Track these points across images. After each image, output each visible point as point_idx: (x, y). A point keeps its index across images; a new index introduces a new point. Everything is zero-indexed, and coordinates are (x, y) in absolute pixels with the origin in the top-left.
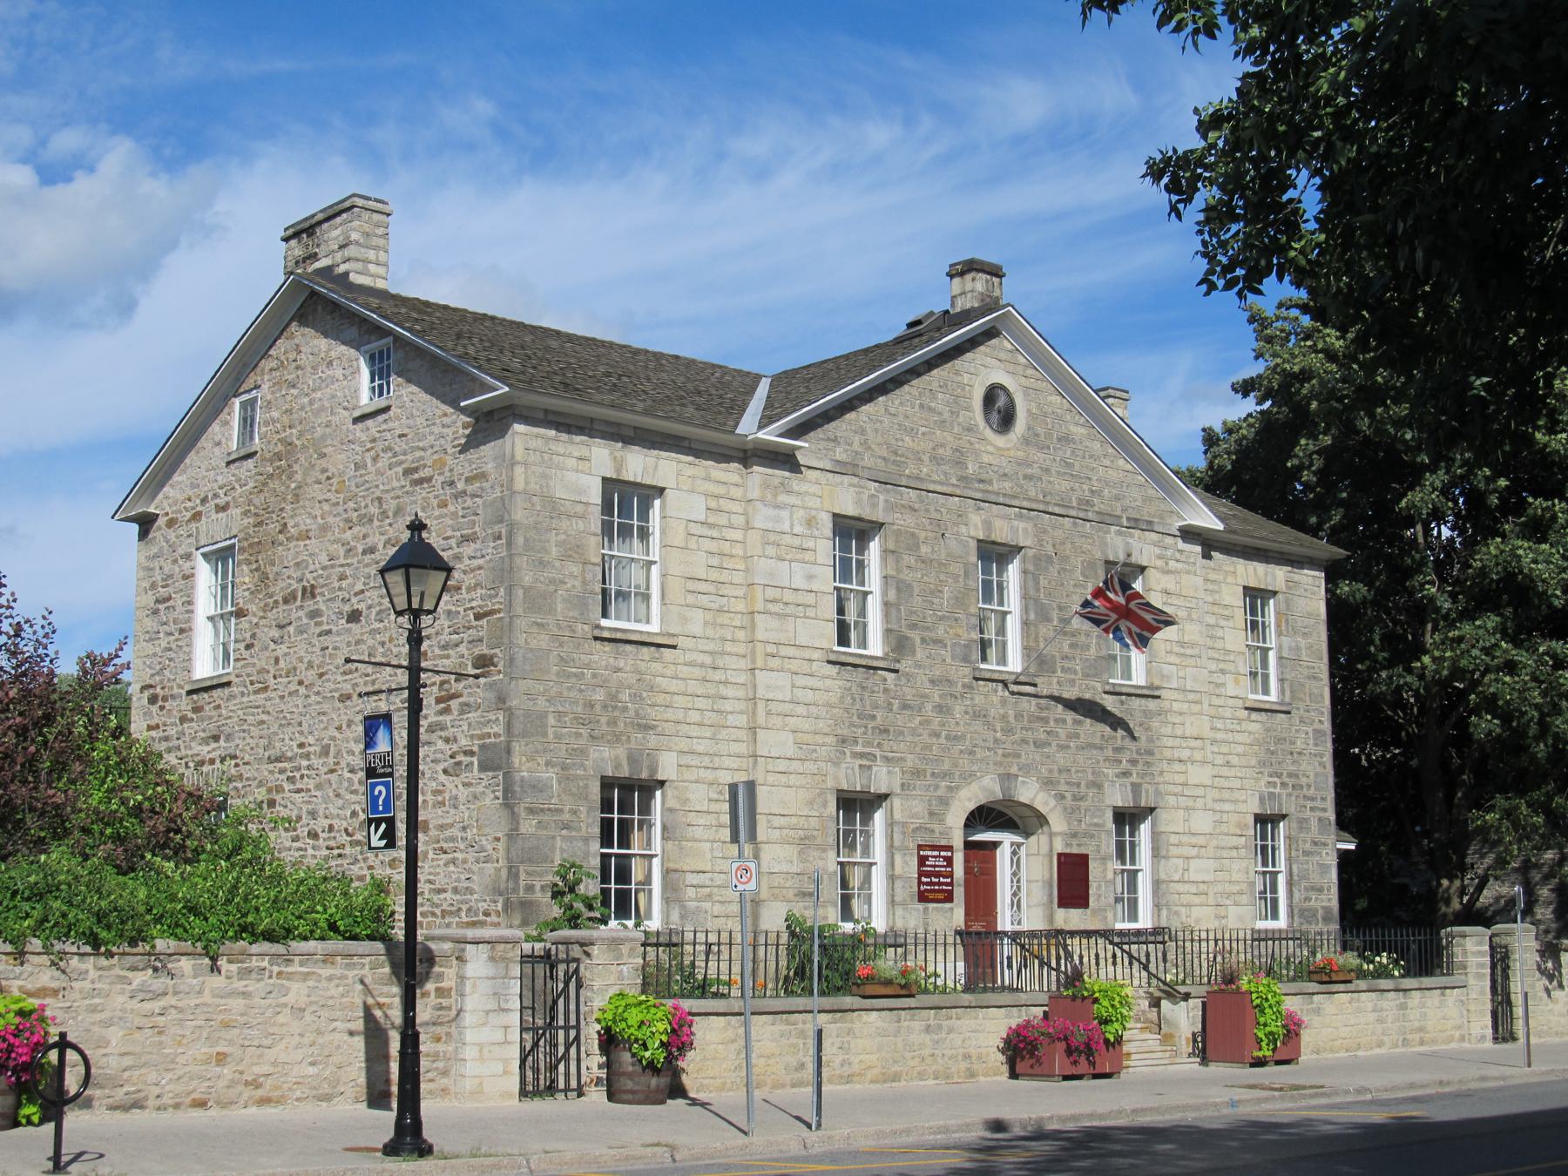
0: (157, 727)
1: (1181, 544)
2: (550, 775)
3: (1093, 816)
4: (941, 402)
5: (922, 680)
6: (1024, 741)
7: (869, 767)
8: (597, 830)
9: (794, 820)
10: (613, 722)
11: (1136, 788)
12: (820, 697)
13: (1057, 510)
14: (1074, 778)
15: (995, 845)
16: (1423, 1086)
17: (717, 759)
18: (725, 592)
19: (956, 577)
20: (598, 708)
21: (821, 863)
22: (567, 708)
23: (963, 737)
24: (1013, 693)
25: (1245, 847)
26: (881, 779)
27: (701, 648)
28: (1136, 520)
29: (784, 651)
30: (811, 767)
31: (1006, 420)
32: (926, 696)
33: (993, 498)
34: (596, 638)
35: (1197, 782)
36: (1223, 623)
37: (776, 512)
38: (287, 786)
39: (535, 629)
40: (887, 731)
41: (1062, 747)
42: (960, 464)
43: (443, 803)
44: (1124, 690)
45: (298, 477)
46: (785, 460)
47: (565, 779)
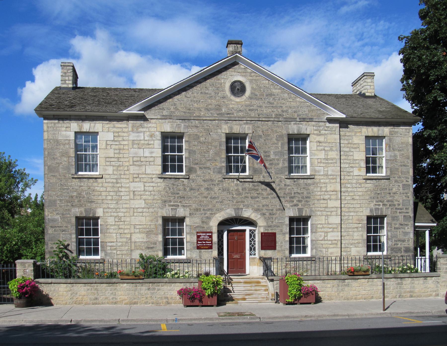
1: (328, 124)
2: (58, 217)
3: (279, 220)
4: (211, 90)
5: (200, 181)
6: (246, 197)
9: (145, 226)
10: (79, 201)
12: (160, 189)
15: (245, 231)
16: (294, 317)
17: (118, 210)
18: (122, 160)
19: (216, 147)
20: (74, 198)
22: (63, 198)
23: (218, 197)
24: (241, 182)
25: (362, 227)
26: (180, 212)
27: (112, 177)
32: (202, 185)
33: (233, 119)
34: (73, 178)
35: (332, 206)
36: (353, 150)
37: (138, 134)
39: (52, 177)
40: (184, 197)
46: (143, 118)
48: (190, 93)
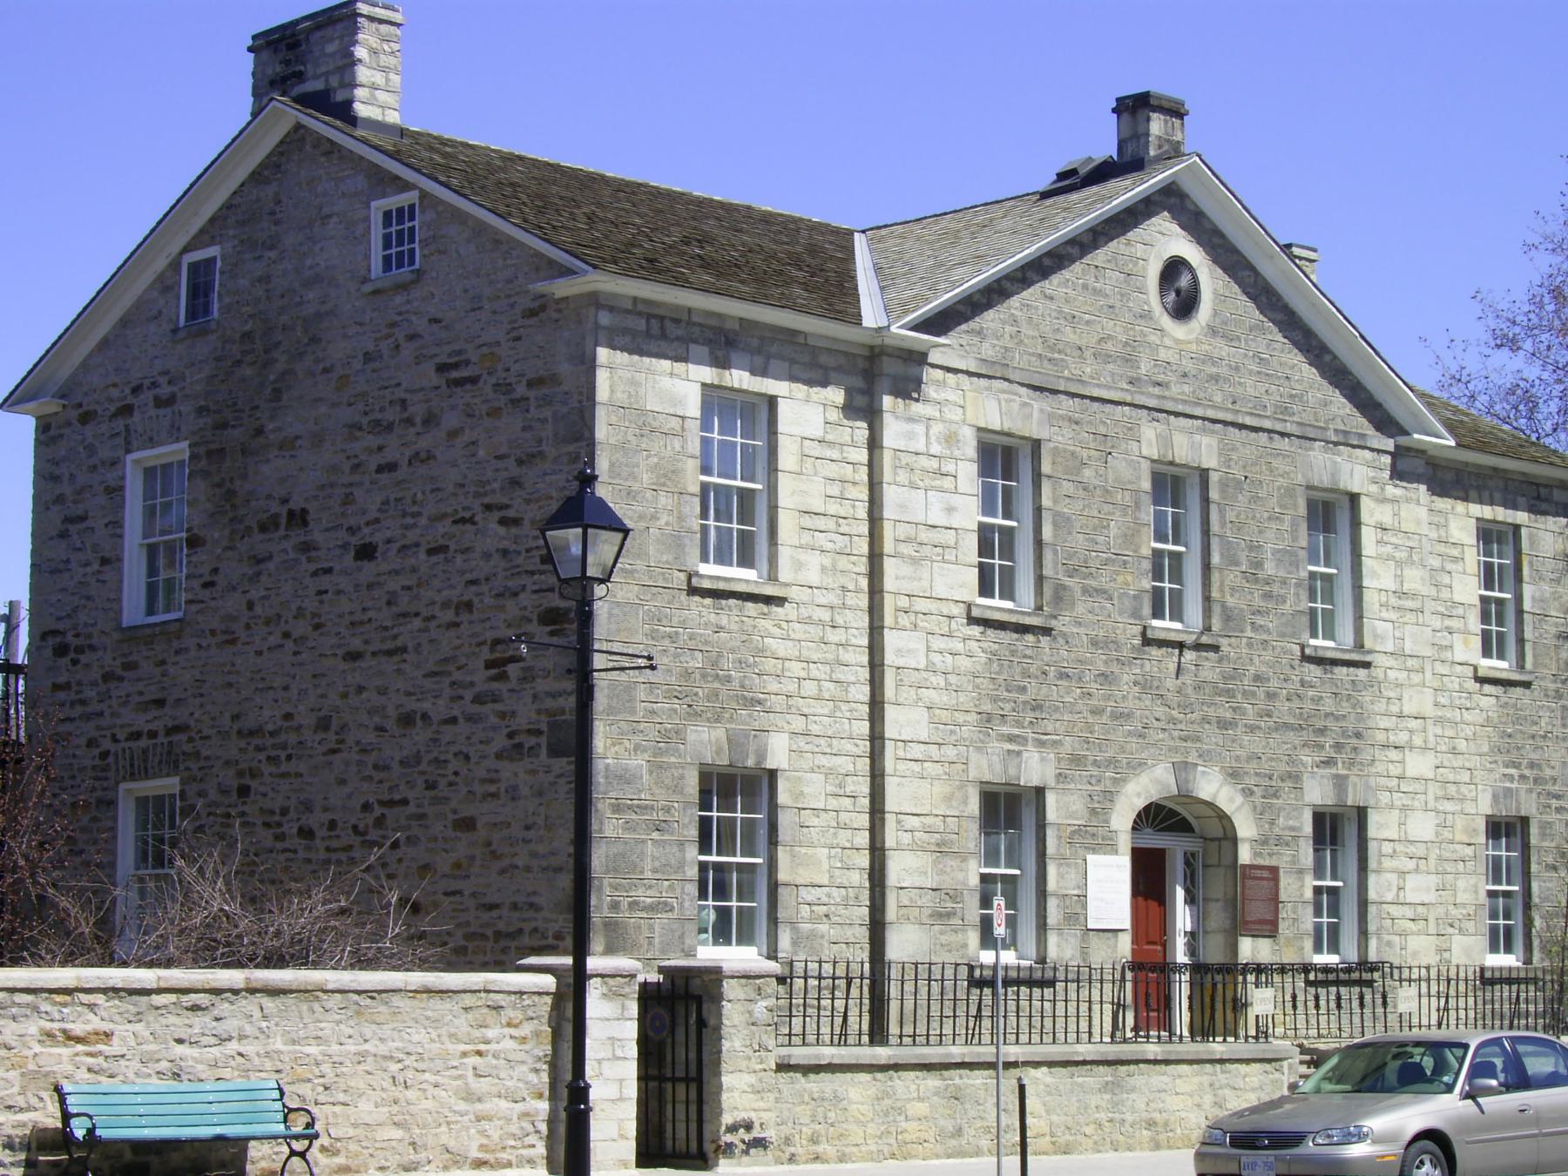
0: (66, 686)
2: (639, 762)
3: (1288, 817)
6: (1205, 720)
7: (1019, 753)
8: (693, 833)
11: (1340, 782)
12: (964, 663)
13: (1249, 421)
14: (1265, 767)
21: (960, 876)
28: (1345, 433)
29: (922, 605)
30: (950, 752)
31: (1185, 307)
33: (1170, 406)
36: (1449, 566)
38: (267, 769)
41: (1252, 729)
42: (1129, 361)
43: (494, 796)
44: (1329, 655)
45: (280, 366)
47: (656, 767)
48: (1054, 284)
